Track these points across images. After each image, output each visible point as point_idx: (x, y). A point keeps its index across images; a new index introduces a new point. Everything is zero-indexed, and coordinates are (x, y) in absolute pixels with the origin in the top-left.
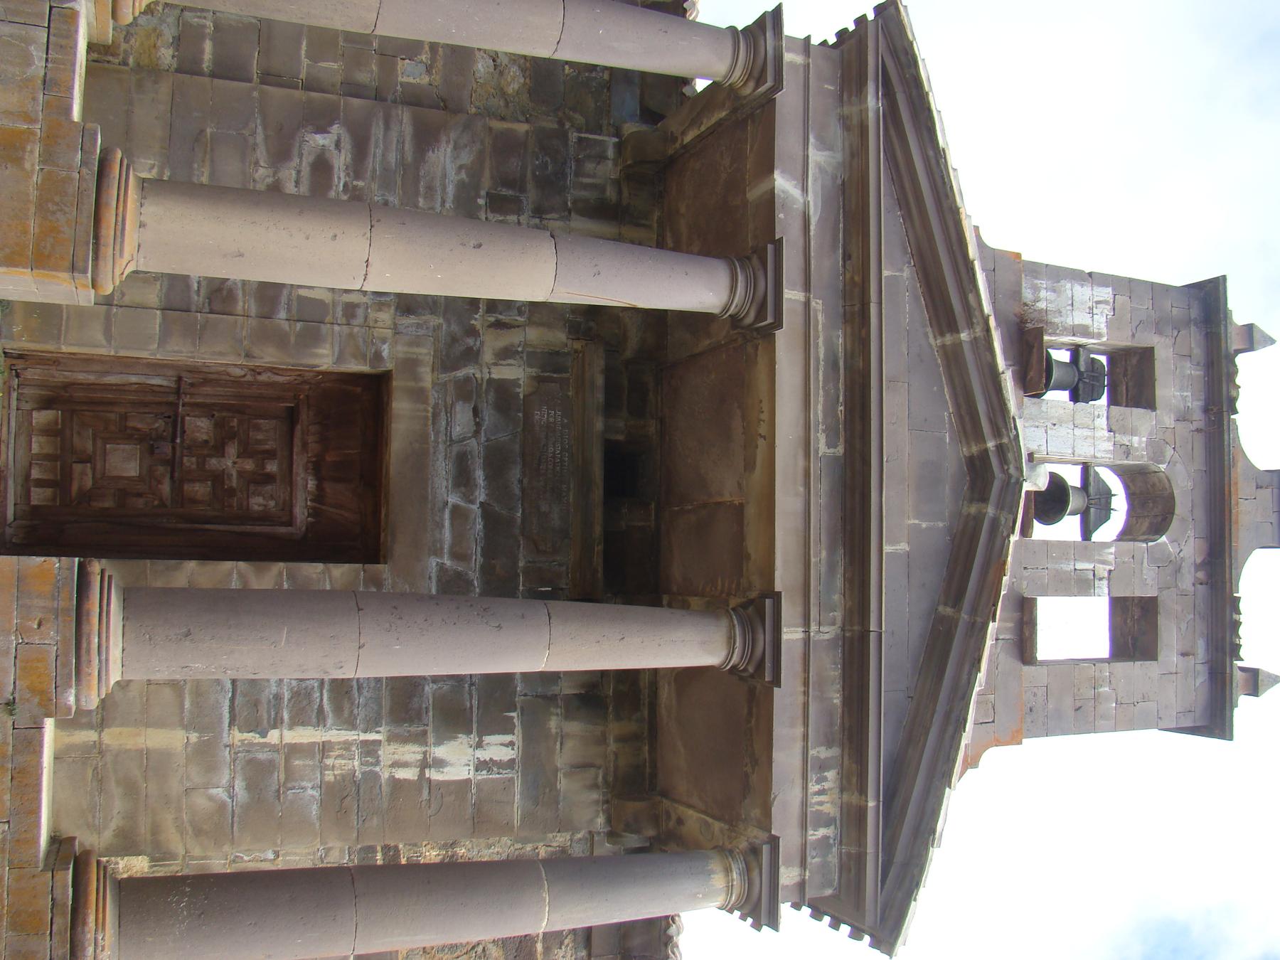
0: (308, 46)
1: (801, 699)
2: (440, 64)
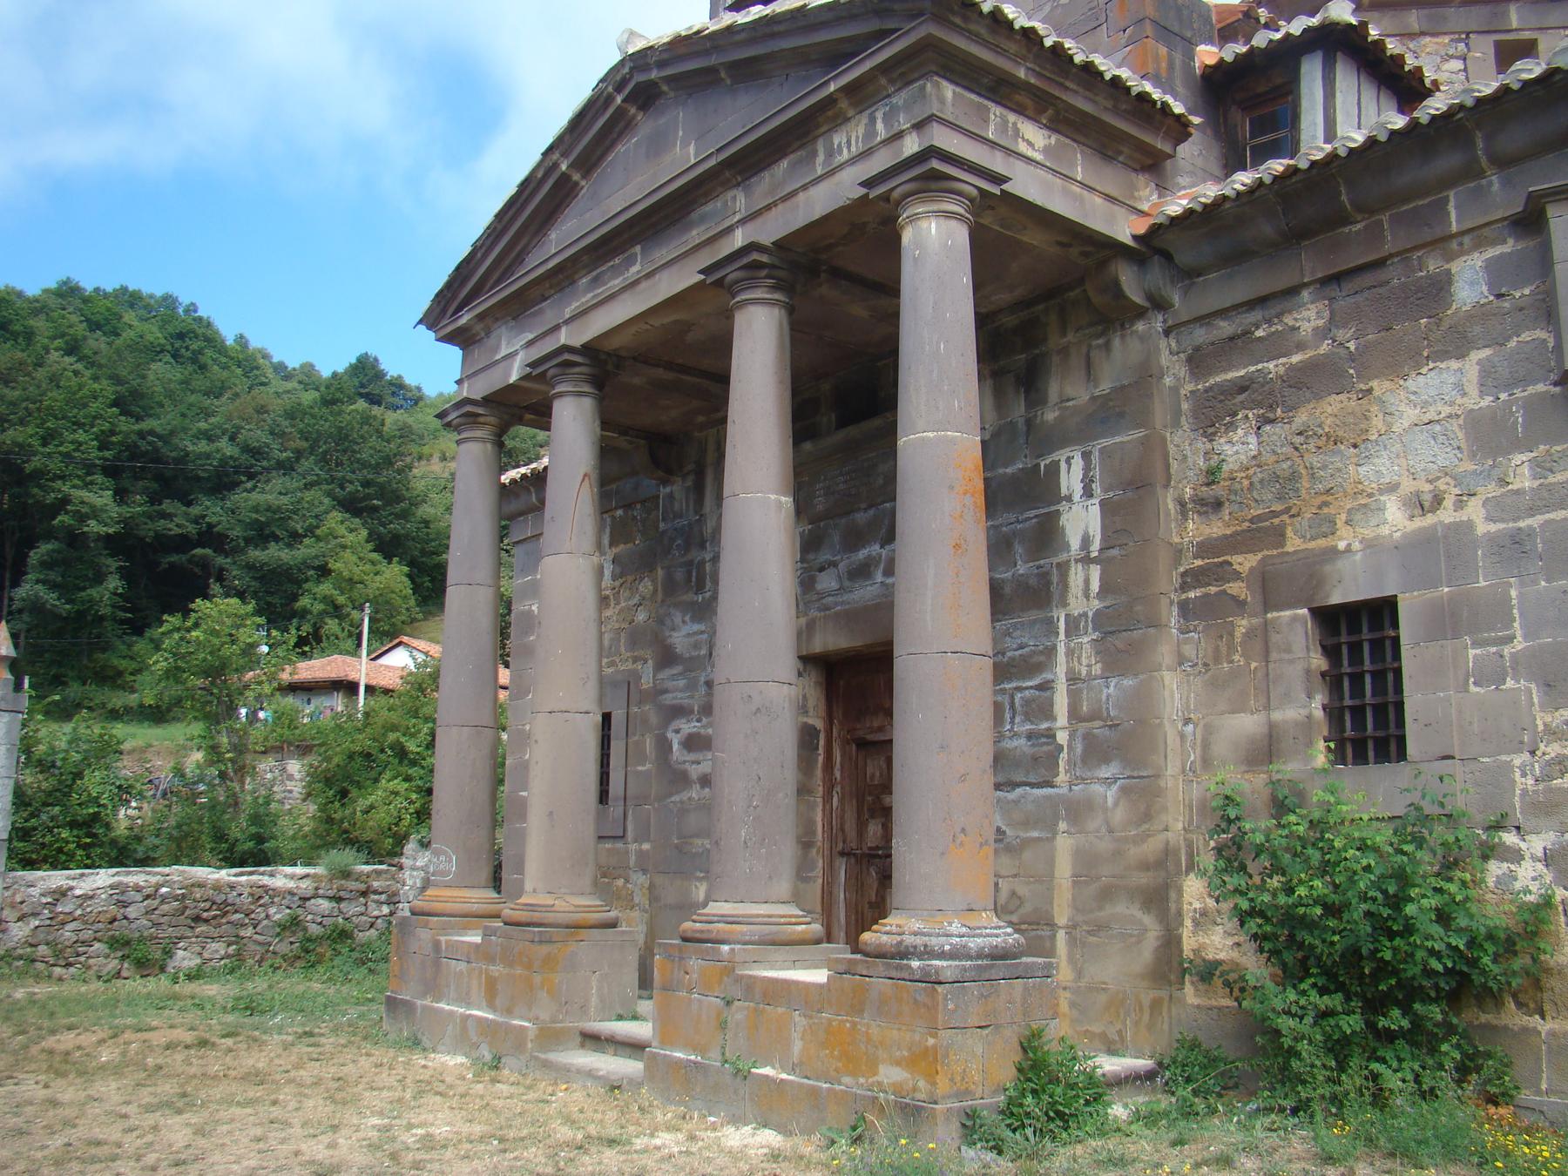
1: (780, 207)
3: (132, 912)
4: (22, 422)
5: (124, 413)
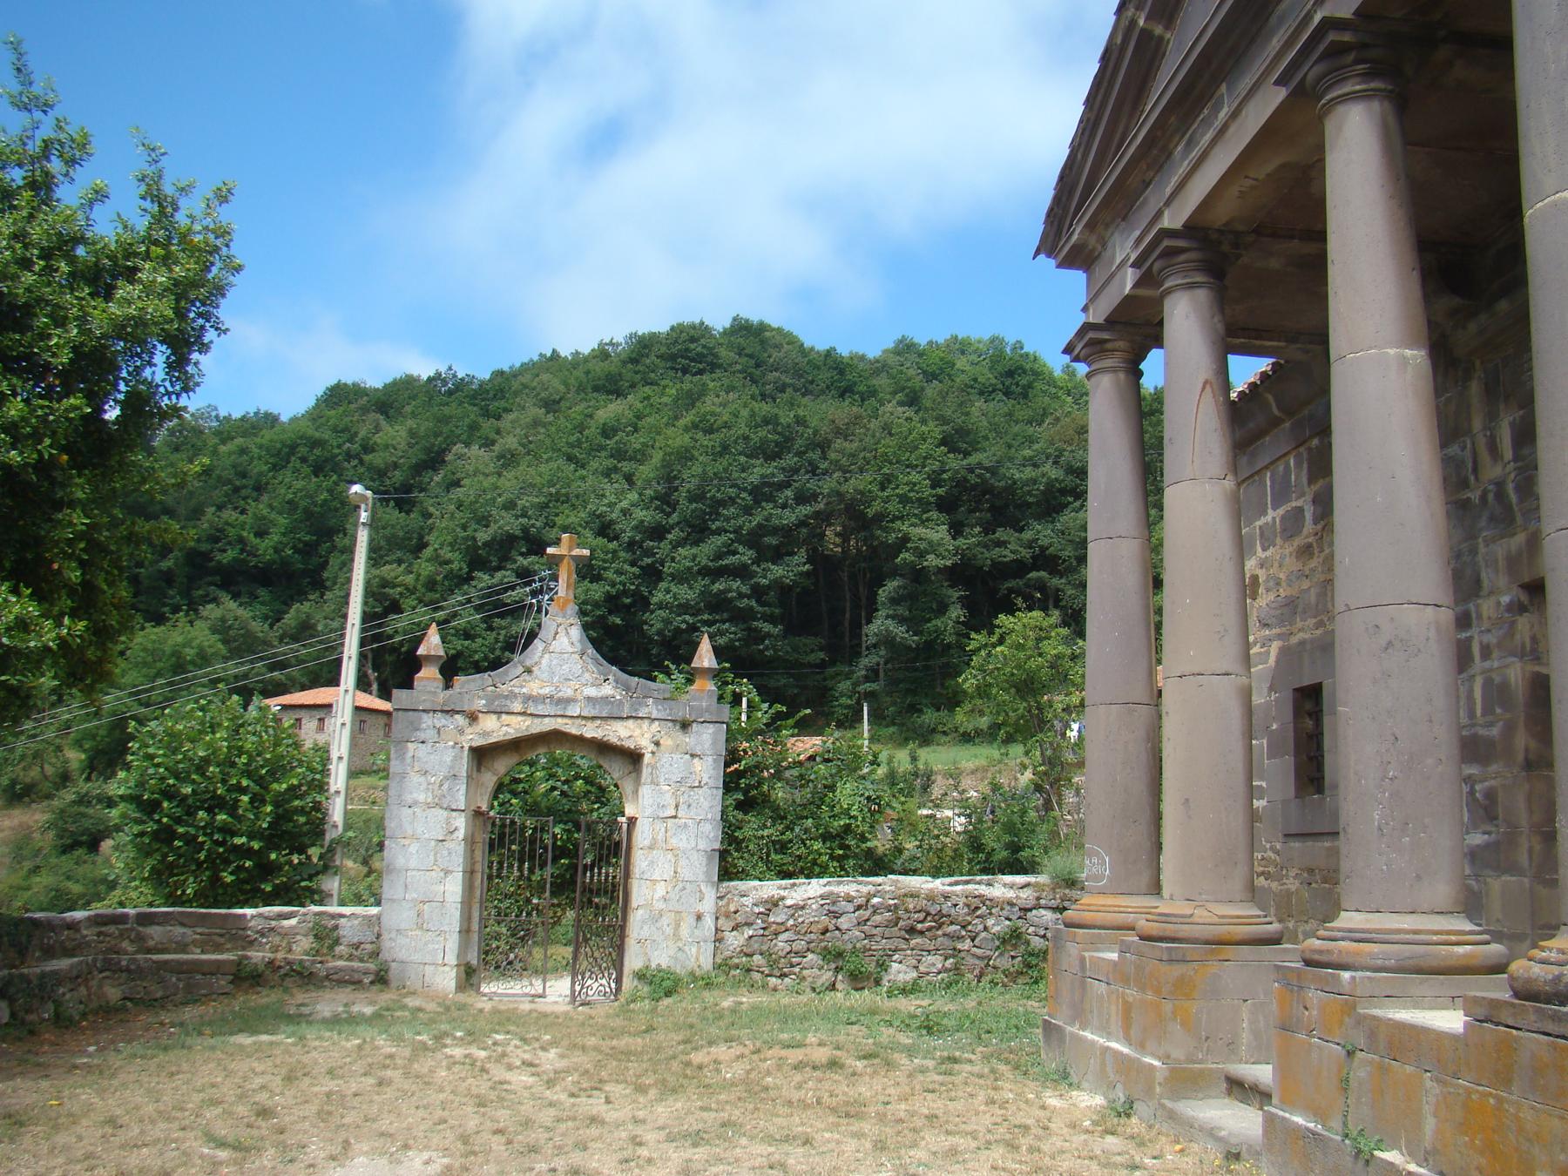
3: (844, 922)
4: (861, 471)
5: (953, 450)
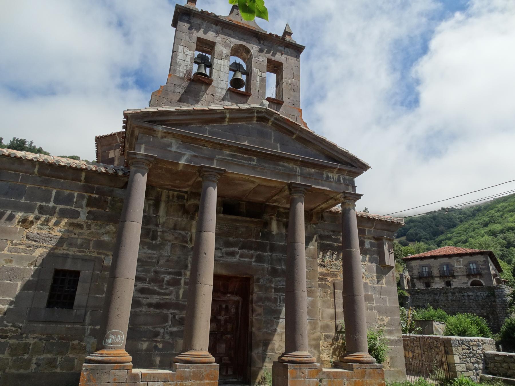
0: (98, 294)
2: (105, 252)
